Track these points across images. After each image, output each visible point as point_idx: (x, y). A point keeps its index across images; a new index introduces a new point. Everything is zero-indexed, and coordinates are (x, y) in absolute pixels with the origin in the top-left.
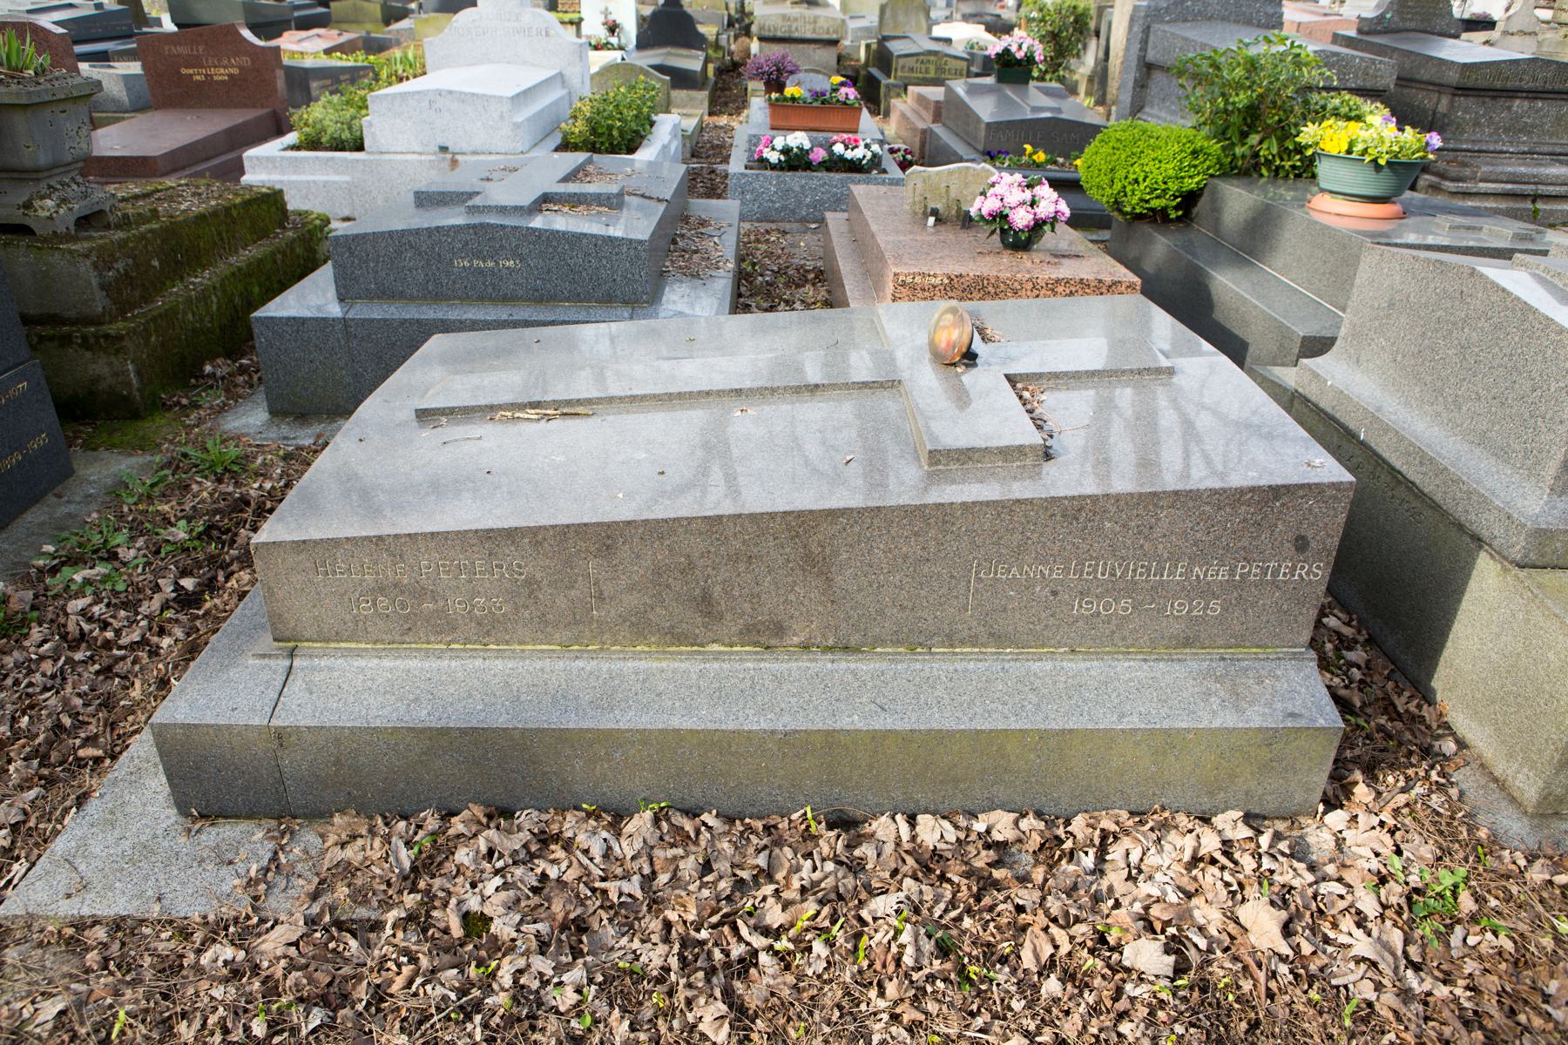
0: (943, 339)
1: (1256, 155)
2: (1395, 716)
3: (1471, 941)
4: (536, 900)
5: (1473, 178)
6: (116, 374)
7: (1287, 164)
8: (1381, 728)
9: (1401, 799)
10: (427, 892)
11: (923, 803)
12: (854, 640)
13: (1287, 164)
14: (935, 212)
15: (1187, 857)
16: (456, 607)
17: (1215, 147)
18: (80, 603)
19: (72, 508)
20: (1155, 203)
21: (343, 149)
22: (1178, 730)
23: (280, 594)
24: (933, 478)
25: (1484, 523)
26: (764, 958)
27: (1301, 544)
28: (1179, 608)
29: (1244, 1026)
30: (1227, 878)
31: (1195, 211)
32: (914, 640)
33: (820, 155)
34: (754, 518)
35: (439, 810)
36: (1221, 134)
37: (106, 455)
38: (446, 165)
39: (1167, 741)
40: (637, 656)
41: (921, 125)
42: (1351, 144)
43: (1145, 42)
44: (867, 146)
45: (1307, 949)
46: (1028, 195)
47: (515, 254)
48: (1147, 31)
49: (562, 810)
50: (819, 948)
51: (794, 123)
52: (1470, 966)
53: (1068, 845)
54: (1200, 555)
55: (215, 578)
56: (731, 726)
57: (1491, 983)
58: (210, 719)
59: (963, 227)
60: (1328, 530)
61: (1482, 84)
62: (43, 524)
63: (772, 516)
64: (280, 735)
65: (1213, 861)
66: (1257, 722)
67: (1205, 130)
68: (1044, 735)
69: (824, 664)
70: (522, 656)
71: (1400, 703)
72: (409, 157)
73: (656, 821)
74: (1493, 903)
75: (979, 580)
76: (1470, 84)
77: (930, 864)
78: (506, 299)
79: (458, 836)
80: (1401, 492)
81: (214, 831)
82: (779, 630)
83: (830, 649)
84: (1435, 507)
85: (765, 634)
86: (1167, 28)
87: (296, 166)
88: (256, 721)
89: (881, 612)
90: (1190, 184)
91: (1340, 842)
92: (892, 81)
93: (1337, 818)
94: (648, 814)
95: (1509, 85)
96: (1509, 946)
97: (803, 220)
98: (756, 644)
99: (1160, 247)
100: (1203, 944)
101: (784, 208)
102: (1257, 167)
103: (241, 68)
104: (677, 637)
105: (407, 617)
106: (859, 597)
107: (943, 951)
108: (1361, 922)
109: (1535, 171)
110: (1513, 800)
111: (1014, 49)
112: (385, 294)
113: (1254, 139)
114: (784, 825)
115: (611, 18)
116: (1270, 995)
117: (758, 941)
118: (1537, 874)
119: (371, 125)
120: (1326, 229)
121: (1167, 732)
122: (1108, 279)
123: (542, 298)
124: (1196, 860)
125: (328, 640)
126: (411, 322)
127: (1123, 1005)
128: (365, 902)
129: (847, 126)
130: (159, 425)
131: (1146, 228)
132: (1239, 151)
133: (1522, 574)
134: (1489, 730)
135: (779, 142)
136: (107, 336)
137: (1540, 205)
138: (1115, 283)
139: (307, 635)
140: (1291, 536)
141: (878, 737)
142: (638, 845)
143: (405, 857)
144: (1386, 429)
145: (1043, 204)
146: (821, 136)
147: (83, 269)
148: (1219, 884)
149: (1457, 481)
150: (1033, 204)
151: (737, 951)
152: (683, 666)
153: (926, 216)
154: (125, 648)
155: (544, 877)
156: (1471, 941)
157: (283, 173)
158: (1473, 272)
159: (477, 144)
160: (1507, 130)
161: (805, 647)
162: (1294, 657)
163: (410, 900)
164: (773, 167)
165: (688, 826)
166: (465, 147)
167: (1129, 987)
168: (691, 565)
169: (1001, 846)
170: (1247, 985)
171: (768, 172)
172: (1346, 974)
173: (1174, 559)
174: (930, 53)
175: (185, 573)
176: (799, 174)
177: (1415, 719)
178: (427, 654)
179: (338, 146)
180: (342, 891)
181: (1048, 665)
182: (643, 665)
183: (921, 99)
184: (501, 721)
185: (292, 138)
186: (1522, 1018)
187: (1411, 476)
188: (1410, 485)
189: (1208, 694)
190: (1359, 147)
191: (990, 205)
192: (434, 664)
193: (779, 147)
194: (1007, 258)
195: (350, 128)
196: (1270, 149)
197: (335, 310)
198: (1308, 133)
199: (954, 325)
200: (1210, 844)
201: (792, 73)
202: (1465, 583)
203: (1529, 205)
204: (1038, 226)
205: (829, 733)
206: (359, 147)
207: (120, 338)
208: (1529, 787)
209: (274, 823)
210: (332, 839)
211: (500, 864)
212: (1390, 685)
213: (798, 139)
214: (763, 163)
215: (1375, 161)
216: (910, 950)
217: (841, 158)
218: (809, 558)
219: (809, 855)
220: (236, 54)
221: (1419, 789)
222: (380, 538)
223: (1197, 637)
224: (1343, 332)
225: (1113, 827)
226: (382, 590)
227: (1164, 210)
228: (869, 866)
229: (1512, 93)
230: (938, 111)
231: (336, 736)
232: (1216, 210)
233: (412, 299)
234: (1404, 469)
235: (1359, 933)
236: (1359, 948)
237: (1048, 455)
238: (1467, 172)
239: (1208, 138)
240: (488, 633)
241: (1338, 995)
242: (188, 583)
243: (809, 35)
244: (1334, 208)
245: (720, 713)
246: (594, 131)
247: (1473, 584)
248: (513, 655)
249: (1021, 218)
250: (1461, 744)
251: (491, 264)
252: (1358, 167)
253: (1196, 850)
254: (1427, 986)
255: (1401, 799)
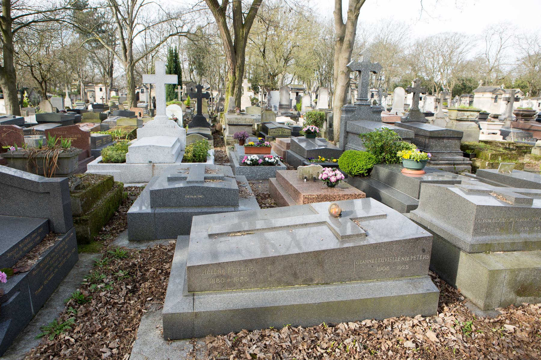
0: (333, 211)
1: (384, 158)
2: (449, 292)
3: (476, 336)
4: (266, 349)
5: (438, 160)
6: (84, 231)
7: (393, 160)
8: (447, 295)
9: (455, 309)
10: (239, 350)
11: (349, 319)
12: (328, 281)
13: (393, 160)
14: (306, 178)
15: (411, 325)
16: (235, 279)
17: (374, 157)
18: (103, 293)
19: (83, 269)
20: (361, 172)
21: (118, 162)
22: (405, 295)
23: (192, 279)
24: (342, 242)
25: (460, 244)
26: (325, 355)
27: (424, 251)
28: (399, 268)
29: (433, 357)
30: (422, 328)
31: (371, 173)
32: (342, 280)
33: (261, 161)
34: (307, 253)
35: (234, 332)
36: (375, 153)
37: (83, 254)
38: (151, 167)
39: (402, 298)
40: (279, 289)
41: (283, 150)
42: (410, 156)
43: (346, 126)
44: (274, 158)
45: (442, 340)
46: (334, 173)
47: (202, 194)
48: (346, 123)
49: (264, 329)
50: (337, 350)
51: (252, 152)
52: (477, 341)
53: (384, 325)
54: (403, 255)
55: (136, 285)
56: (306, 303)
57: (482, 343)
58: (178, 311)
59: (314, 181)
60: (429, 248)
61: (435, 136)
62: (77, 274)
63: (311, 252)
64: (196, 314)
65: (417, 325)
66: (421, 292)
67: (371, 152)
68: (375, 299)
69: (323, 287)
70: (251, 291)
71: (450, 289)
72: (140, 164)
73: (289, 329)
74: (479, 327)
75: (356, 264)
76: (433, 136)
77: (355, 332)
78: (199, 206)
79: (241, 337)
80: (440, 240)
81: (175, 343)
82: (312, 280)
83: (323, 284)
84: (449, 242)
85: (308, 282)
86: (351, 122)
87: (103, 168)
88: (190, 311)
89: (335, 274)
90: (369, 167)
91: (444, 320)
92: (269, 136)
93: (442, 315)
94: (287, 327)
95: (442, 136)
96: (484, 335)
97: (257, 180)
98: (306, 284)
99: (364, 183)
100: (420, 342)
101: (252, 176)
102: (385, 161)
103: (78, 138)
104: (288, 284)
105: (223, 283)
106: (330, 271)
107: (365, 348)
108: (452, 334)
109: (453, 157)
110: (479, 308)
111: (311, 129)
112: (165, 206)
113: (383, 154)
114: (318, 328)
115: (175, 117)
116: (437, 350)
117: (323, 351)
118: (487, 321)
119: (128, 155)
120: (408, 178)
121: (402, 296)
122: (357, 194)
123: (208, 205)
124: (413, 326)
125: (202, 291)
126: (173, 213)
127: (407, 355)
128: (222, 355)
129: (267, 152)
130: (95, 245)
131: (359, 179)
132: (380, 157)
133: (470, 255)
134: (470, 293)
135: (249, 158)
136: (83, 220)
137: (456, 166)
138: (359, 195)
139: (197, 290)
140: (421, 249)
141: (339, 302)
142: (286, 335)
143: (230, 344)
144: (434, 226)
145: (338, 175)
146: (260, 155)
147: (77, 201)
148: (420, 330)
149: (452, 236)
150: (335, 175)
151: (318, 354)
152: (291, 290)
153: (303, 179)
154: (121, 304)
155: (265, 344)
156: (476, 336)
157: (99, 170)
158: (447, 189)
159: (161, 160)
160: (444, 147)
161: (317, 284)
162: (426, 277)
163: (234, 353)
164: (248, 165)
165: (296, 330)
166: (157, 161)
167: (407, 351)
168: (292, 265)
169: (369, 327)
170: (432, 348)
171: (247, 166)
172: (452, 344)
173: (397, 256)
174: (280, 128)
175: (127, 284)
176: (256, 166)
177: (454, 293)
178: (228, 293)
179: (117, 161)
180: (216, 353)
181: (373, 284)
182: (281, 291)
183: (281, 142)
184: (251, 306)
185: (100, 158)
186: (489, 349)
187: (442, 236)
188: (442, 238)
189: (409, 287)
190: (412, 157)
191: (324, 176)
192: (230, 295)
193: (250, 159)
194: (330, 189)
195: (120, 156)
196: (388, 156)
197: (149, 210)
198: (399, 154)
199: (336, 208)
200: (416, 322)
201: (247, 137)
202: (458, 259)
203: (453, 166)
204: (337, 181)
205: (328, 303)
206: (124, 161)
207: (87, 220)
208: (481, 304)
209: (190, 340)
210: (208, 342)
211: (254, 342)
212: (447, 286)
213: (255, 157)
214: (245, 164)
215: (417, 160)
216: (358, 348)
217: (268, 162)
218: (318, 262)
219: (326, 334)
220: (76, 134)
221: (458, 307)
222: (219, 263)
223: (404, 275)
224: (419, 203)
225: (393, 321)
226: (218, 277)
227: (363, 173)
228: (340, 335)
229: (443, 138)
230: (288, 146)
231: (210, 313)
232: (377, 173)
233: (172, 207)
234: (440, 235)
235: (452, 336)
236: (454, 339)
237: (367, 236)
238: (436, 158)
239: (372, 154)
240: (243, 286)
241: (451, 348)
242: (129, 287)
243: (244, 124)
244: (408, 172)
245: (302, 300)
246: (194, 156)
247: (460, 259)
248: (249, 292)
249: (333, 179)
250: (465, 298)
251: (195, 197)
252: (412, 162)
253: (413, 323)
254: (469, 345)
255: (455, 309)
